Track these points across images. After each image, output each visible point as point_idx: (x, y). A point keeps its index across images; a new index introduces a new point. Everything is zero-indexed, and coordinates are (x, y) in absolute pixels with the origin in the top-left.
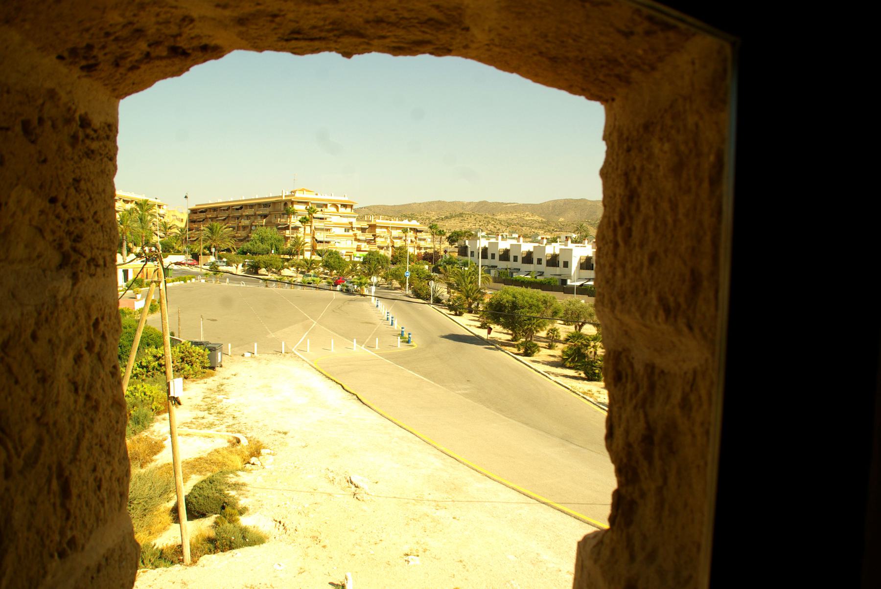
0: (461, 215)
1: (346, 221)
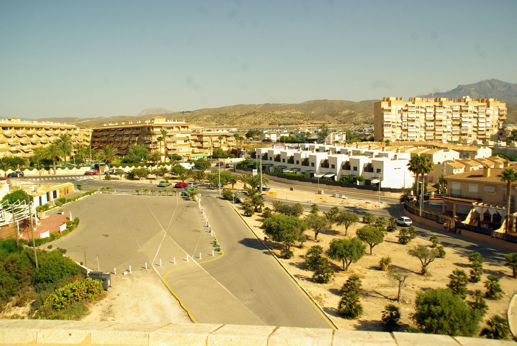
0: (254, 113)
1: (184, 136)
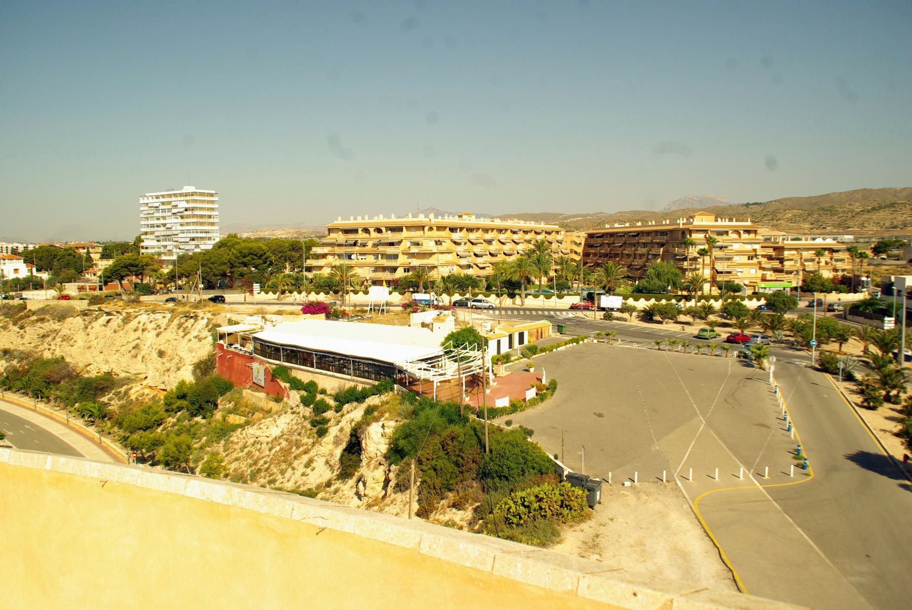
0: (892, 205)
1: (748, 247)
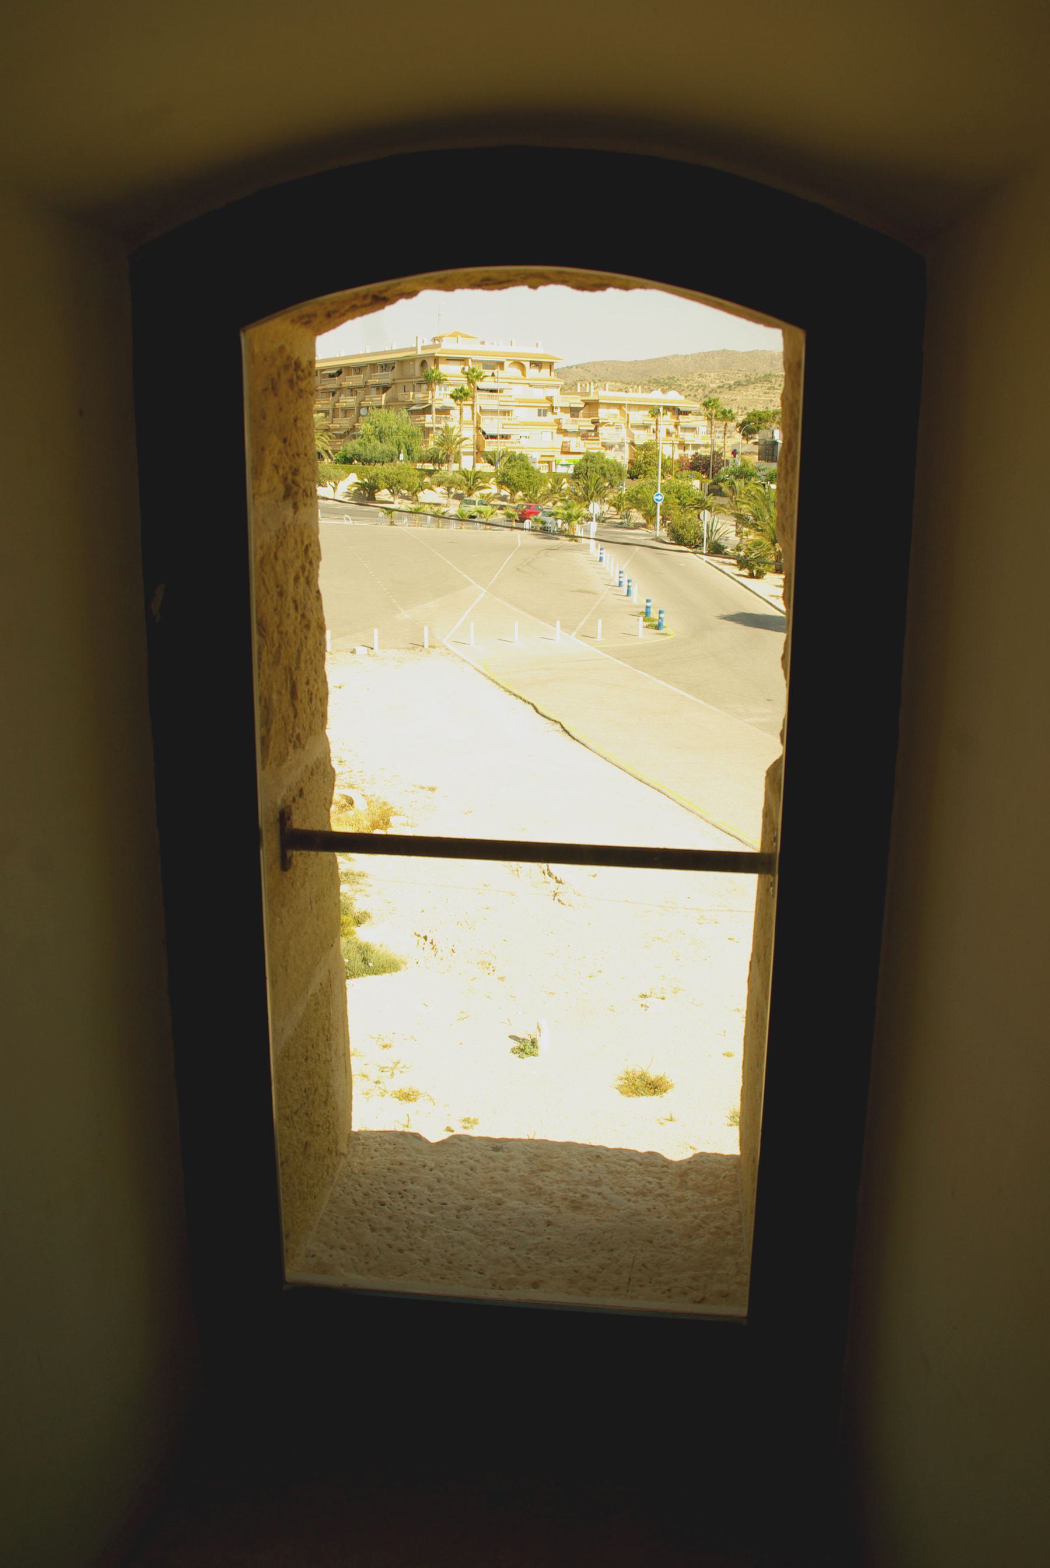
1: (540, 394)
